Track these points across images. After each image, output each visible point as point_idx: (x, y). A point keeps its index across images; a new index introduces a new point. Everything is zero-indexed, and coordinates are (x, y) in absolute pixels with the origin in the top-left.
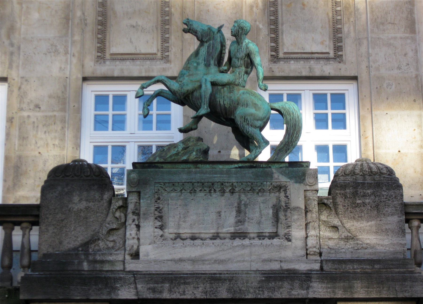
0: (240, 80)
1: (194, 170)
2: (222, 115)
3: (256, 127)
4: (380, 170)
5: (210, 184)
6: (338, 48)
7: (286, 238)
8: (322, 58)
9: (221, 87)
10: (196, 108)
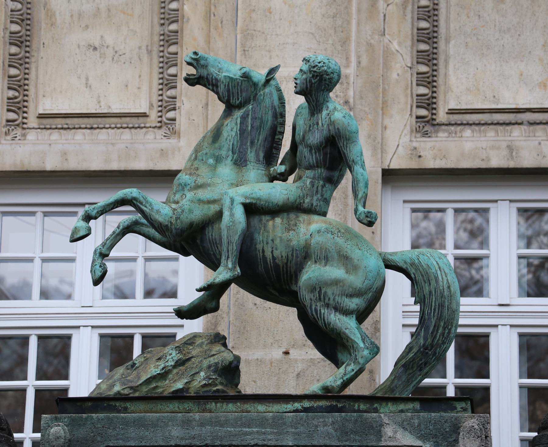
0: (315, 198)
1: (197, 416)
2: (272, 280)
3: (346, 312)
8: (541, 123)
9: (268, 217)
10: (212, 262)
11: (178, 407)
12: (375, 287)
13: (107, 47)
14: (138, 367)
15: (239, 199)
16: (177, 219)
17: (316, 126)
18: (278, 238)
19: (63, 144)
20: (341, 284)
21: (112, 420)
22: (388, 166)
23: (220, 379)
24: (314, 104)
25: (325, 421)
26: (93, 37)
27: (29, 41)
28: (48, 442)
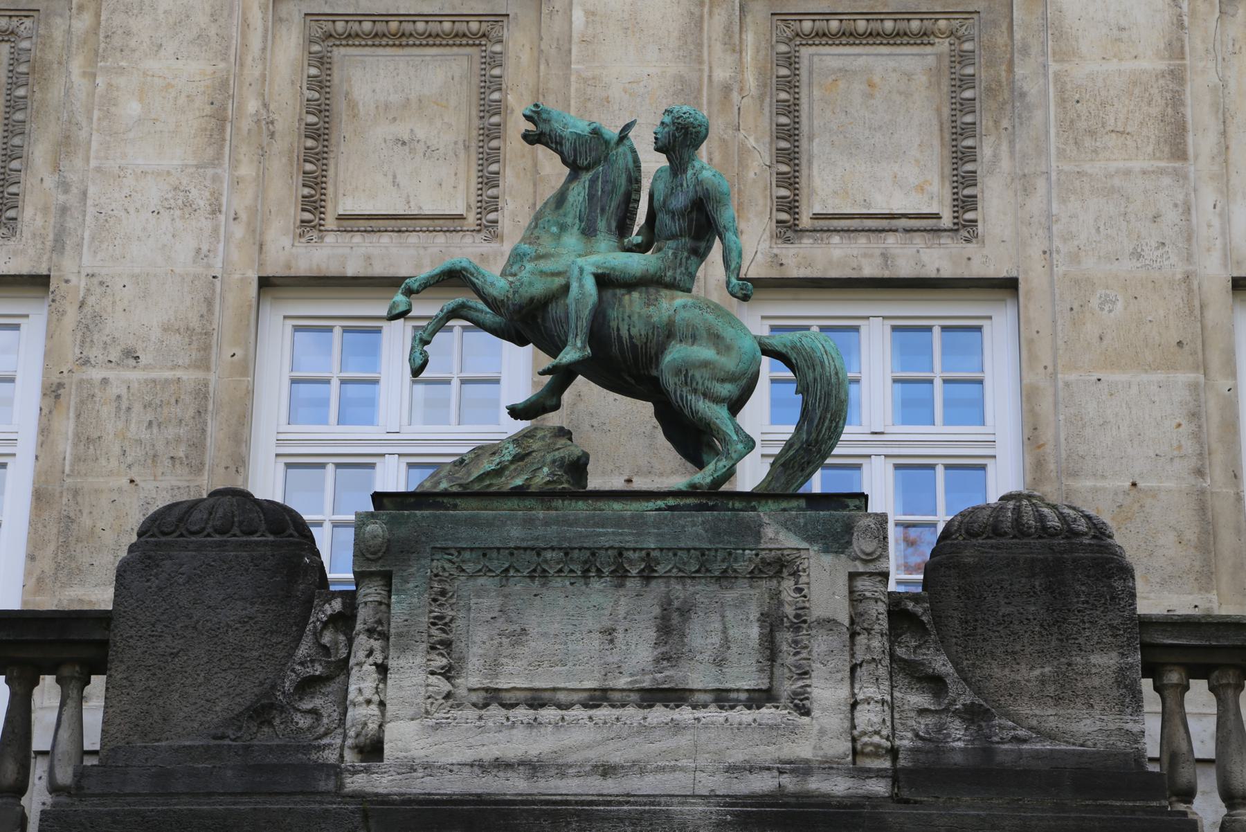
0: (678, 271)
1: (541, 514)
2: (626, 366)
3: (717, 400)
4: (1069, 525)
5: (588, 553)
6: (965, 204)
7: (796, 705)
8: (918, 230)
9: (623, 291)
10: (552, 346)
12: (750, 372)
16: (514, 293)
18: (636, 314)
23: (565, 477)
26: (402, 130)
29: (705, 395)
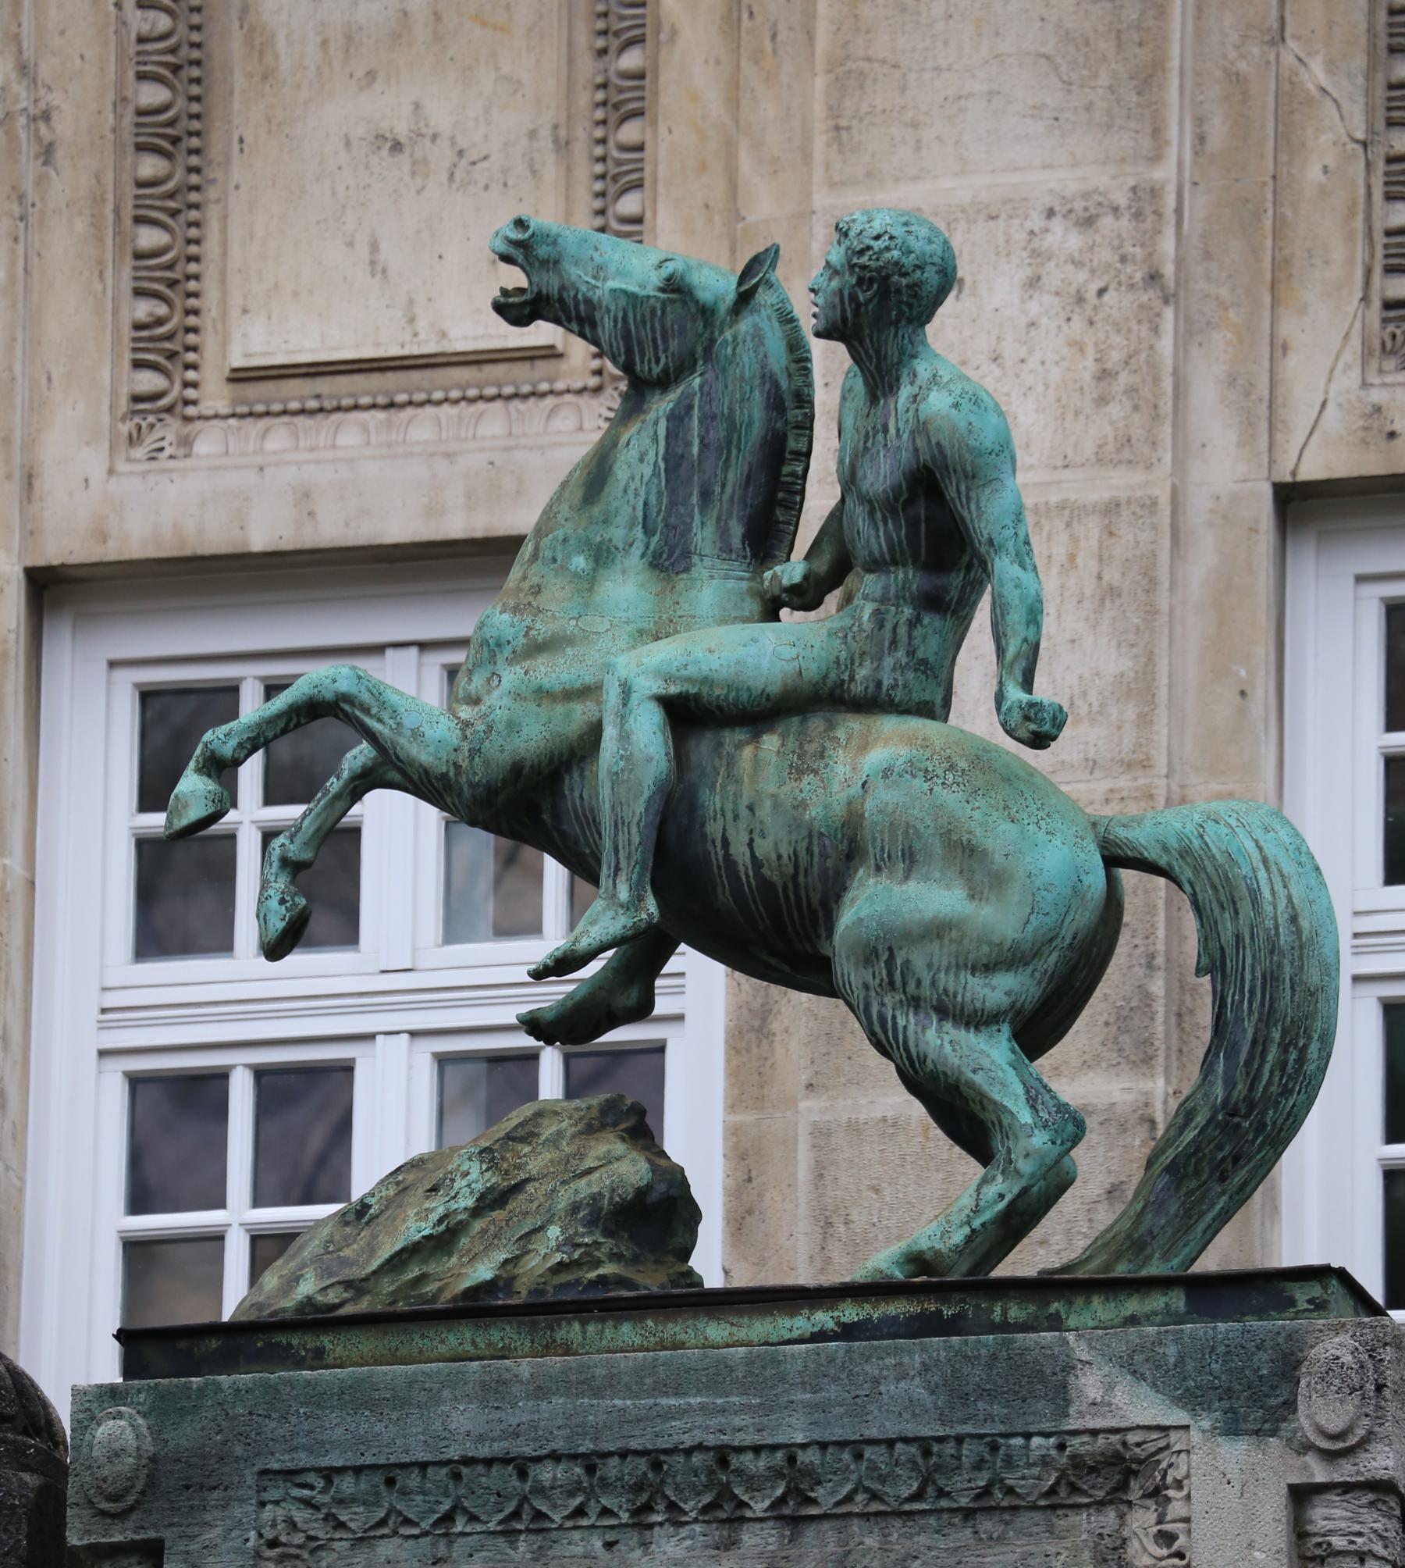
0: (888, 662)
3: (977, 1020)
5: (642, 1464)
9: (740, 735)
11: (473, 1343)
13: (434, 138)
14: (377, 1216)
15: (648, 686)
16: (474, 752)
17: (880, 437)
18: (768, 797)
19: (299, 464)
20: (954, 934)
21: (277, 1391)
22: (1294, 473)
23: (608, 1244)
24: (872, 368)
25: (900, 1364)
26: (388, 107)
27: (198, 134)
28: (89, 1467)
29: (943, 1011)
